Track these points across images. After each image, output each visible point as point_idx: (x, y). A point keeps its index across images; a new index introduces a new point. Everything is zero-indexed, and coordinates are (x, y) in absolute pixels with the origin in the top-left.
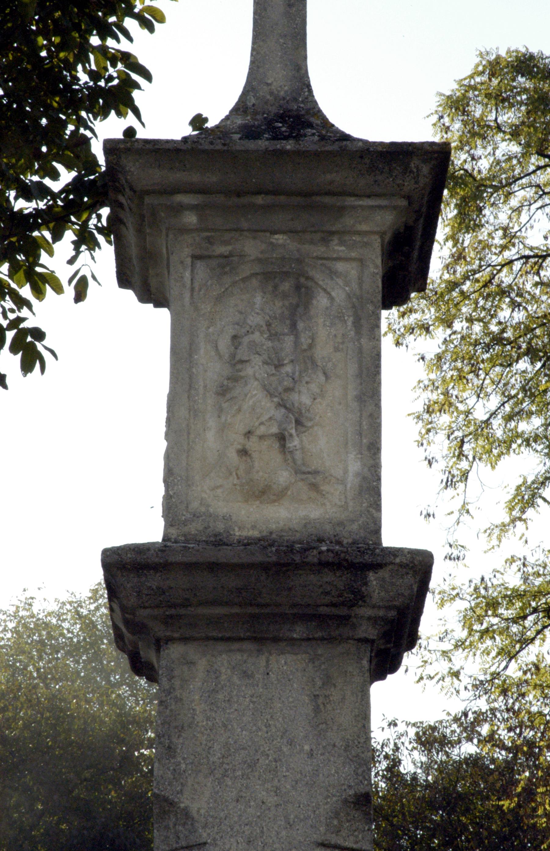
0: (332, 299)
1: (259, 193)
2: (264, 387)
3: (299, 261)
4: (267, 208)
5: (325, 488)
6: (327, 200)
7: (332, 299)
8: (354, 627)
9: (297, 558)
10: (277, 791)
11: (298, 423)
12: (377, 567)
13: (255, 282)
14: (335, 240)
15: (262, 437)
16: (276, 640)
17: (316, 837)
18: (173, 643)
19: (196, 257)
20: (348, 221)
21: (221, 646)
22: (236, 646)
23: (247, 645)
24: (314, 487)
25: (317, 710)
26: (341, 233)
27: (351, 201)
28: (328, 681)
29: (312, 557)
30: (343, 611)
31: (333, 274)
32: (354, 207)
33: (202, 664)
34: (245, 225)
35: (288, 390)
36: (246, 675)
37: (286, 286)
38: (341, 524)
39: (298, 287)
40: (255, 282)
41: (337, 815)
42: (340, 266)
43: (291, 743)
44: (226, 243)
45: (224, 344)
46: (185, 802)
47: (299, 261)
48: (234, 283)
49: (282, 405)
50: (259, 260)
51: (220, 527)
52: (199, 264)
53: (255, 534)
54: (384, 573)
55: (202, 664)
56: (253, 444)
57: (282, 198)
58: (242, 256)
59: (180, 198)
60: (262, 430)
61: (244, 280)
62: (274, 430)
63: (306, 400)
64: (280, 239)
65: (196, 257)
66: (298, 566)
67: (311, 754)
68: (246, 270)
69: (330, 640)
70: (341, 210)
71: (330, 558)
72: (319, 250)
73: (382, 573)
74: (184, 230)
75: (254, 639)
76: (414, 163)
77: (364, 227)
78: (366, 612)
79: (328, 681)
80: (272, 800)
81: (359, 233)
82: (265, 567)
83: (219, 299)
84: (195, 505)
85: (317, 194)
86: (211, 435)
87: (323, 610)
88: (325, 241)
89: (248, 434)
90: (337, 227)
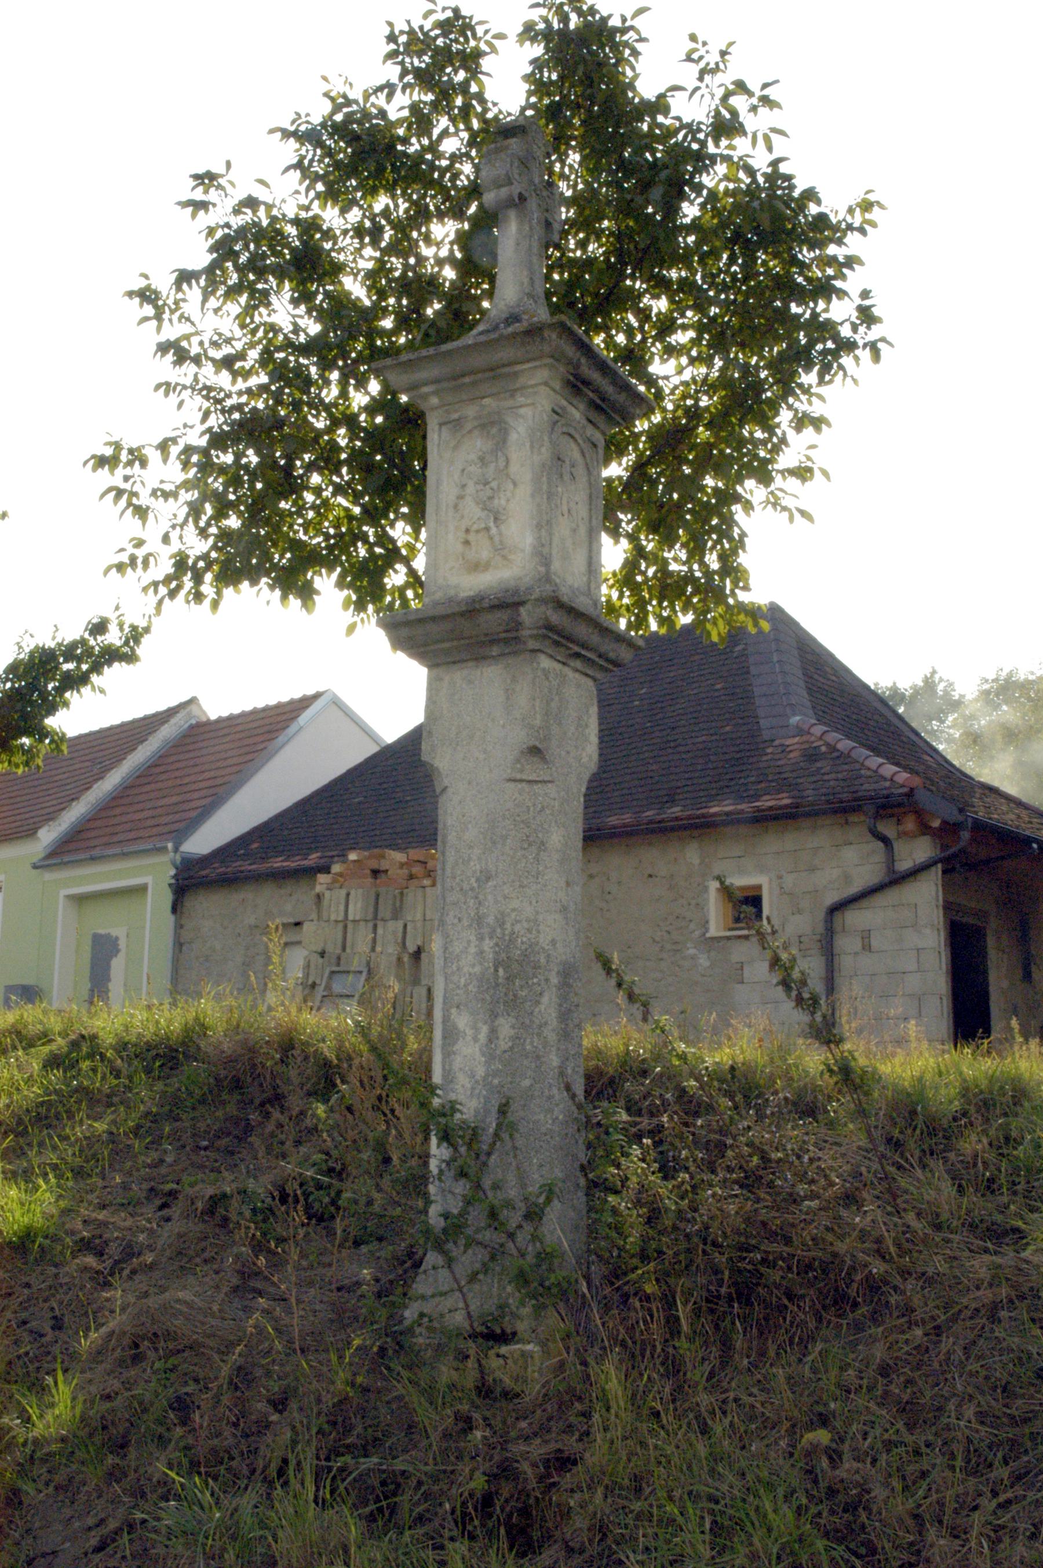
1: (463, 376)
3: (499, 413)
4: (474, 384)
5: (512, 557)
6: (506, 370)
8: (525, 643)
9: (477, 606)
10: (485, 751)
11: (496, 519)
12: (521, 603)
14: (518, 394)
15: (478, 531)
16: (484, 658)
19: (441, 425)
20: (522, 380)
22: (464, 665)
23: (470, 664)
24: (504, 557)
25: (508, 698)
27: (518, 368)
28: (514, 679)
29: (486, 604)
32: (523, 371)
33: (447, 678)
34: (464, 397)
35: (491, 498)
36: (470, 682)
38: (520, 578)
40: (476, 432)
41: (518, 761)
42: (522, 411)
43: (493, 720)
44: (456, 411)
47: (499, 413)
48: (463, 436)
49: (484, 509)
50: (475, 418)
51: (452, 592)
52: (444, 428)
54: (528, 606)
55: (447, 678)
56: (471, 537)
57: (480, 375)
60: (475, 527)
61: (470, 432)
63: (503, 502)
65: (441, 425)
67: (503, 726)
68: (469, 426)
69: (514, 653)
70: (516, 374)
71: (496, 602)
72: (510, 403)
75: (476, 659)
76: (546, 333)
77: (533, 382)
78: (526, 633)
79: (514, 679)
80: (482, 756)
81: (532, 386)
82: (462, 614)
83: (456, 448)
84: (440, 581)
85: (504, 366)
87: (504, 635)
88: (512, 396)
89: (467, 531)
90: (518, 385)
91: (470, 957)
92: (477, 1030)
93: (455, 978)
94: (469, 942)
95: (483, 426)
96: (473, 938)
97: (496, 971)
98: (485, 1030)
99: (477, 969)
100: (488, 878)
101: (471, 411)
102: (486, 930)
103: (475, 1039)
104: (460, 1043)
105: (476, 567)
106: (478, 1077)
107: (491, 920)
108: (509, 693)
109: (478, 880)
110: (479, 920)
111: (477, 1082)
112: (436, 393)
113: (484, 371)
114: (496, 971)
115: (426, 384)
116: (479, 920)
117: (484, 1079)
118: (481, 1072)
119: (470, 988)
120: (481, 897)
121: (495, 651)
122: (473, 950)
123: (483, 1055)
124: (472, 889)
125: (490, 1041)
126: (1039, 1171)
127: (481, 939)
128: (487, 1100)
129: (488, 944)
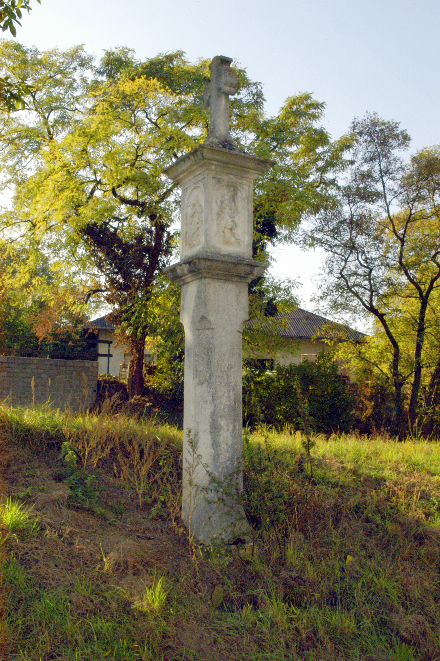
0: (242, 194)
2: (229, 216)
7: (242, 194)
9: (241, 262)
13: (225, 187)
16: (230, 280)
17: (237, 329)
18: (230, 284)
20: (248, 175)
21: (216, 280)
22: (220, 281)
23: (223, 281)
25: (237, 299)
26: (246, 178)
27: (251, 171)
28: (240, 292)
29: (244, 262)
30: (246, 276)
31: (243, 188)
37: (232, 189)
39: (234, 190)
40: (225, 187)
42: (245, 186)
44: (220, 175)
45: (219, 202)
46: (209, 318)
51: (219, 251)
53: (226, 253)
58: (223, 180)
59: (213, 162)
62: (230, 227)
64: (232, 176)
66: (240, 264)
68: (224, 183)
70: (248, 172)
71: (248, 263)
72: (240, 181)
73: (258, 268)
74: (211, 170)
77: (251, 177)
80: (228, 319)
86: (215, 226)
89: (225, 227)
91: (225, 398)
92: (227, 425)
93: (219, 406)
94: (225, 392)
95: (228, 185)
96: (226, 391)
97: (235, 404)
98: (231, 426)
99: (228, 403)
100: (232, 368)
101: (225, 178)
102: (231, 388)
103: (228, 430)
104: (222, 432)
105: (227, 243)
106: (229, 445)
107: (232, 384)
108: (238, 297)
109: (227, 368)
110: (228, 384)
111: (229, 446)
112: (216, 165)
113: (218, 161)
114: (235, 404)
115: (215, 161)
116: (228, 384)
117: (232, 445)
118: (230, 443)
119: (226, 410)
120: (229, 375)
121: (235, 279)
122: (226, 395)
123: (231, 436)
124: (225, 371)
125: (234, 431)
126: (438, 466)
127: (229, 391)
128: (233, 453)
129: (232, 394)
